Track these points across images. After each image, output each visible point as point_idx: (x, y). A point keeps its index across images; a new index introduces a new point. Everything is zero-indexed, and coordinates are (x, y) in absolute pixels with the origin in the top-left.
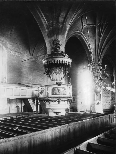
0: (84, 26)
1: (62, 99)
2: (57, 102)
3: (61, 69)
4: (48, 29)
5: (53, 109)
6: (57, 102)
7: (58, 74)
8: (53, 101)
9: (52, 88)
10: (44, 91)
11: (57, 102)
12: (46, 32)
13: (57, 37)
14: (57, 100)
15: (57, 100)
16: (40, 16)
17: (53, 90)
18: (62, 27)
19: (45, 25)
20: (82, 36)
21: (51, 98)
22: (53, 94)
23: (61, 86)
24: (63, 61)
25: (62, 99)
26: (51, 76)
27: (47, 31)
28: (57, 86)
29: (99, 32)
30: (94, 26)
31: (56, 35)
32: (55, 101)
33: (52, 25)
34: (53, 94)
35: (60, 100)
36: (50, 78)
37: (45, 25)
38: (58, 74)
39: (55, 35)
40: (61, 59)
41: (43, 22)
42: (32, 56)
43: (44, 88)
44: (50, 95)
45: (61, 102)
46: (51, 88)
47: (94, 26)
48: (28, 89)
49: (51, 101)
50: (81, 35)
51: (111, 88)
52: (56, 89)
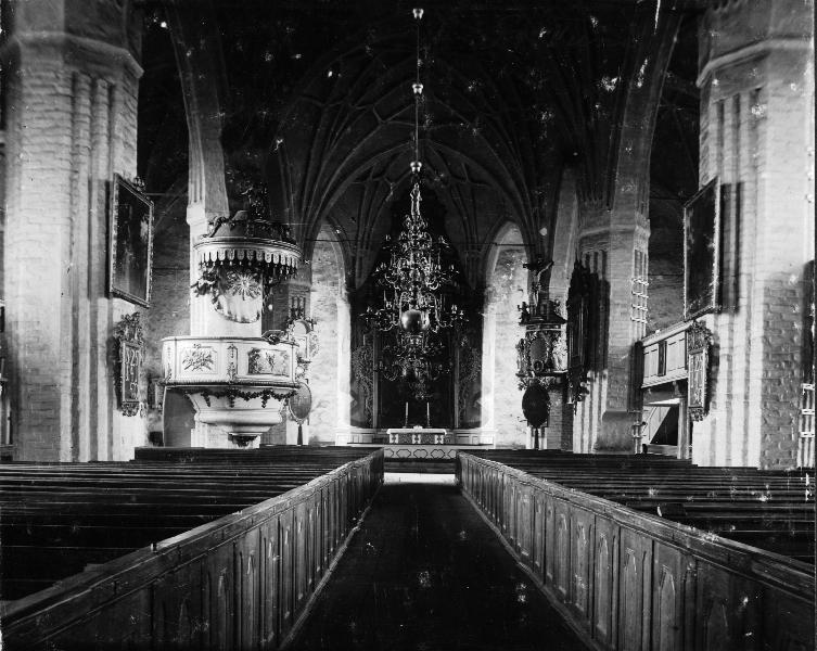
6: (259, 400)
8: (247, 397)
9: (250, 350)
10: (213, 359)
11: (259, 400)
14: (261, 394)
15: (261, 394)
17: (254, 354)
26: (222, 299)
30: (320, 104)
34: (251, 370)
35: (273, 394)
36: (219, 307)
44: (243, 374)
46: (244, 349)
52: (263, 354)
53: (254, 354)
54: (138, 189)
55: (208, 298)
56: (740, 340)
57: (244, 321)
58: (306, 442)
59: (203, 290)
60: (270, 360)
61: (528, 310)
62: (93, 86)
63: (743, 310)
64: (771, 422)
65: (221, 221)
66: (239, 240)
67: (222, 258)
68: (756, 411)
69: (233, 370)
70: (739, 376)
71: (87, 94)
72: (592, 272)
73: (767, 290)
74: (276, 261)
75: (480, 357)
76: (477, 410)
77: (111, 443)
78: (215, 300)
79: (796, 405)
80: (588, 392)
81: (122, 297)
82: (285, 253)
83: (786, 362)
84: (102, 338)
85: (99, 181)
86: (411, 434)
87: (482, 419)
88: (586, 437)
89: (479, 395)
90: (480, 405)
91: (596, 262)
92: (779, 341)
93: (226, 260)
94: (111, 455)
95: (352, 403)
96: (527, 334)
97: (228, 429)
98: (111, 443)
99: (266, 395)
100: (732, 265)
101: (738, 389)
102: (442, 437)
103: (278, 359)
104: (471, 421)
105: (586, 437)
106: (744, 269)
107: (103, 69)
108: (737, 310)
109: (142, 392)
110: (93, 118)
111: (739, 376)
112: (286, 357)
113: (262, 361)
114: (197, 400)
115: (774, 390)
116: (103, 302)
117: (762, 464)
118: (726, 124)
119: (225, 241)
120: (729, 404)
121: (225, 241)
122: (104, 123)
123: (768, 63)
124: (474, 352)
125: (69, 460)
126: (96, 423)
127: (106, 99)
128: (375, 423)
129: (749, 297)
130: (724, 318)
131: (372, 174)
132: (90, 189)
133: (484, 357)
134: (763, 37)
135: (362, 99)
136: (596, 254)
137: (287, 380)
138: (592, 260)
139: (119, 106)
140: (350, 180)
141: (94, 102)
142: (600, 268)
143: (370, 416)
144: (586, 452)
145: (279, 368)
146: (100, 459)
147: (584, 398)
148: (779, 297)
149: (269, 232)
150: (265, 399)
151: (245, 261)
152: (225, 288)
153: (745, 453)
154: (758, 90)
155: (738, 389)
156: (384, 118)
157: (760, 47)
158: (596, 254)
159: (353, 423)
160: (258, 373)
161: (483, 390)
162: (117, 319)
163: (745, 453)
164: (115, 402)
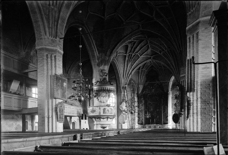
0: (118, 54)
1: (110, 117)
2: (106, 119)
3: (107, 93)
4: (98, 60)
5: (102, 124)
6: (106, 119)
7: (104, 97)
8: (103, 119)
9: (103, 108)
10: (96, 111)
11: (106, 119)
12: (96, 62)
13: (104, 67)
16: (94, 50)
17: (104, 110)
18: (108, 59)
19: (96, 57)
20: (115, 62)
21: (103, 116)
22: (104, 113)
23: (110, 107)
24: (110, 88)
25: (110, 117)
26: (99, 98)
27: (97, 61)
28: (107, 107)
29: (128, 60)
30: (125, 55)
31: (104, 66)
32: (105, 118)
33: (101, 57)
34: (104, 113)
36: (98, 100)
37: (96, 57)
38: (104, 97)
39: (103, 65)
40: (108, 87)
41: (96, 54)
42: (67, 73)
43: (96, 108)
44: (102, 114)
45: (109, 119)
46: (102, 108)
47: (125, 55)
48: (69, 107)
49: (102, 118)
50: (114, 61)
51: (33, 94)
52: (106, 109)
53: (104, 110)
54: (62, 76)
55: (96, 98)
56: (195, 98)
57: (104, 102)
58: (82, 128)
59: (95, 97)
60: (108, 110)
61: (177, 96)
62: (51, 56)
63: (195, 91)
64: (204, 120)
65: (98, 81)
66: (101, 85)
67: (97, 89)
68: (199, 117)
69: (100, 113)
70: (195, 108)
71: (50, 58)
72: (183, 85)
73: (201, 85)
74: (108, 89)
75: (168, 108)
76: (167, 120)
77: (56, 129)
78: (97, 98)
79: (211, 115)
80: (182, 114)
81: (59, 99)
82: (112, 87)
83: (207, 103)
84: (54, 107)
85: (53, 75)
86: (151, 126)
87: (168, 122)
88: (182, 125)
89: (167, 117)
90: (168, 119)
91: (184, 83)
92: (205, 98)
93: (98, 90)
94: (56, 131)
95: (138, 119)
96: (177, 102)
97: (100, 125)
98: (56, 129)
99: (107, 118)
100: (193, 79)
101: (195, 111)
102: (158, 126)
103: (110, 110)
104: (166, 123)
105: (182, 125)
106: (195, 80)
107: (53, 52)
108: (194, 90)
109: (195, 119)
110: (51, 63)
111: (195, 108)
112: (112, 110)
113: (106, 111)
114: (94, 119)
115: (204, 111)
116: (54, 100)
117: (201, 131)
118: (191, 42)
119: (99, 86)
120: (193, 115)
121: (99, 86)
122: (54, 64)
123: (200, 25)
124: (166, 106)
125: (47, 132)
126: (194, 127)
127: (54, 59)
128: (144, 124)
129: (197, 87)
130: (191, 93)
131: (141, 69)
132: (51, 77)
133: (168, 108)
134: (198, 18)
135: (135, 52)
136: (184, 81)
137: (113, 115)
138: (183, 82)
139: (57, 60)
140: (136, 69)
141: (51, 60)
142: (184, 84)
143: (142, 122)
144: (195, 131)
145: (110, 112)
146: (54, 132)
147: (182, 116)
148: (205, 85)
149: (107, 83)
150: (107, 119)
151: (102, 90)
152: (99, 96)
153: (197, 128)
154: (198, 32)
155: (195, 111)
156: (141, 56)
157: (198, 21)
158: (184, 81)
159: (139, 124)
160: (105, 113)
161: (168, 115)
162: (57, 103)
163: (197, 128)
164: (57, 120)
